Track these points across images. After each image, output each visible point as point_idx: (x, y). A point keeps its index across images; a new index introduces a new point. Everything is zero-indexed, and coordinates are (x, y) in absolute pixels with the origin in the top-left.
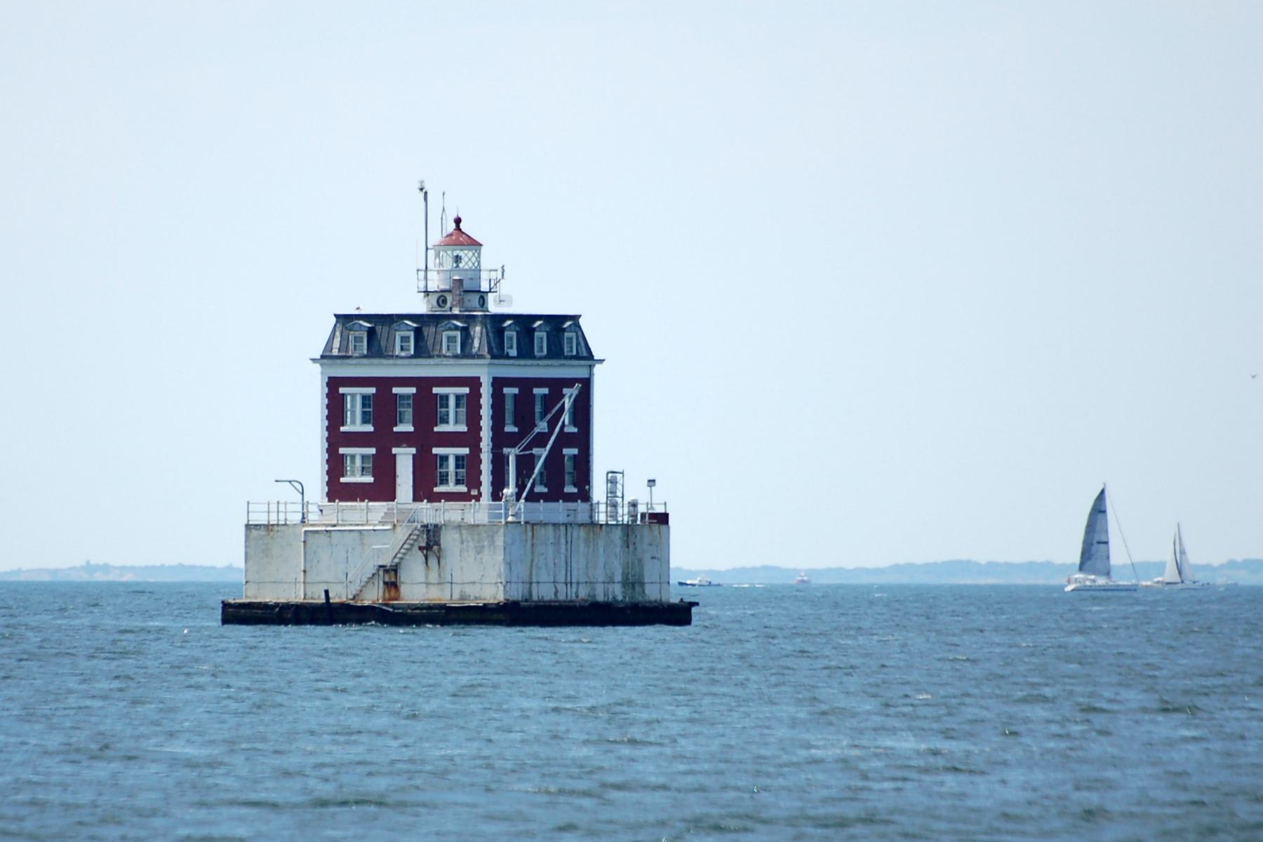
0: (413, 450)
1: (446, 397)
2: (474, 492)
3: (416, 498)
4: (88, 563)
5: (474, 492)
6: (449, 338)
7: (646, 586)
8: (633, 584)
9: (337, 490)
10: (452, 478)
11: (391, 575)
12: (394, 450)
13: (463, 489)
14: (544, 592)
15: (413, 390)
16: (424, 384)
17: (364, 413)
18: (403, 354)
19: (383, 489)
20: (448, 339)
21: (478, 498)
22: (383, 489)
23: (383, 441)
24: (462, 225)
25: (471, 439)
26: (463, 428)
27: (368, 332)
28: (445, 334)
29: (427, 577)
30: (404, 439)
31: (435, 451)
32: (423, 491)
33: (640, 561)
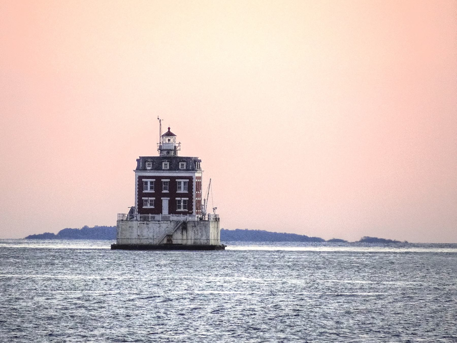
0: (169, 198)
3: (169, 213)
11: (169, 237)
12: (162, 198)
15: (169, 180)
16: (173, 179)
17: (184, 187)
20: (165, 165)
22: (158, 209)
23: (158, 195)
26: (187, 192)
27: (143, 162)
28: (180, 163)
29: (182, 237)
30: (165, 195)
32: (172, 210)
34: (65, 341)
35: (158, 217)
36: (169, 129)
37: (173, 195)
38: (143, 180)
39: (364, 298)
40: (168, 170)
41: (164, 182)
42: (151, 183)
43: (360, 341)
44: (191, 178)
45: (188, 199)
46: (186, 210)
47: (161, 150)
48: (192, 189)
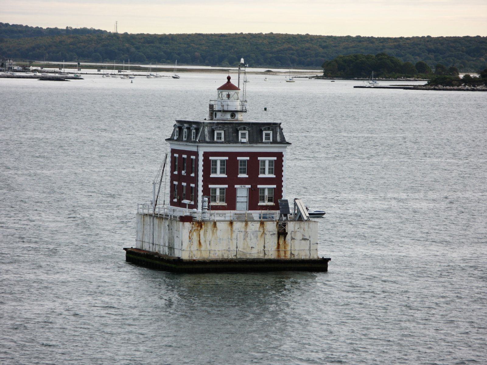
1: (215, 161)
6: (242, 134)
7: (175, 250)
8: (171, 248)
9: (172, 203)
12: (236, 186)
13: (272, 204)
16: (254, 156)
18: (219, 141)
23: (232, 180)
24: (231, 81)
25: (207, 180)
26: (273, 176)
27: (185, 130)
30: (243, 182)
31: (259, 186)
33: (173, 237)
37: (254, 180)
38: (211, 158)
39: (457, 295)
40: (271, 143)
41: (241, 161)
42: (222, 161)
45: (226, 186)
47: (213, 112)
48: (203, 166)
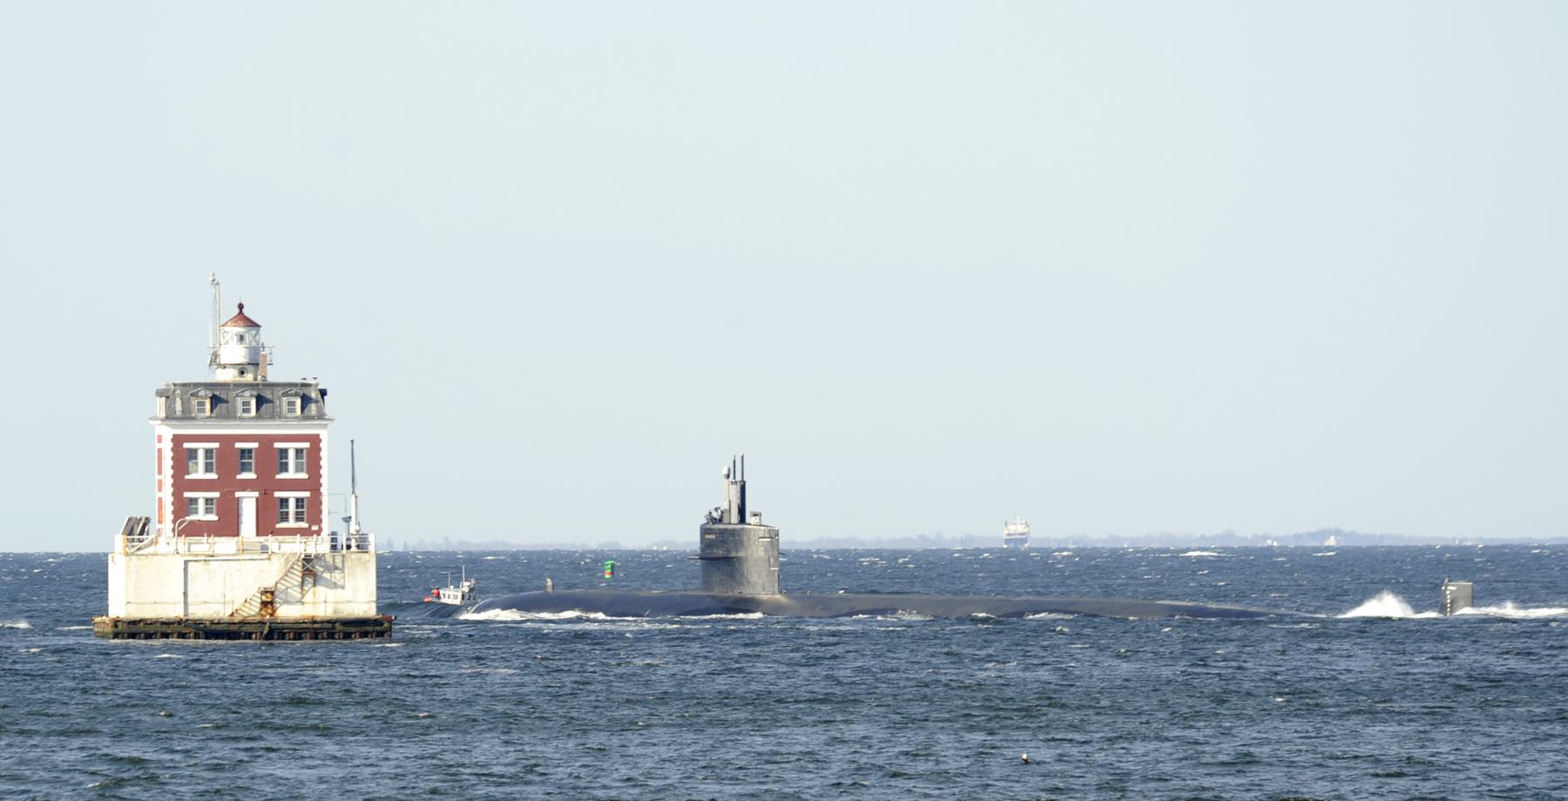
0: (256, 494)
1: (195, 451)
2: (315, 528)
3: (260, 531)
4: (721, 547)
5: (315, 528)
10: (292, 516)
11: (269, 600)
14: (200, 612)
16: (266, 441)
19: (228, 525)
21: (318, 533)
26: (304, 476)
27: (184, 399)
30: (246, 486)
34: (1117, 783)
35: (225, 545)
36: (241, 307)
43: (1518, 798)
44: (315, 440)
46: (304, 525)
